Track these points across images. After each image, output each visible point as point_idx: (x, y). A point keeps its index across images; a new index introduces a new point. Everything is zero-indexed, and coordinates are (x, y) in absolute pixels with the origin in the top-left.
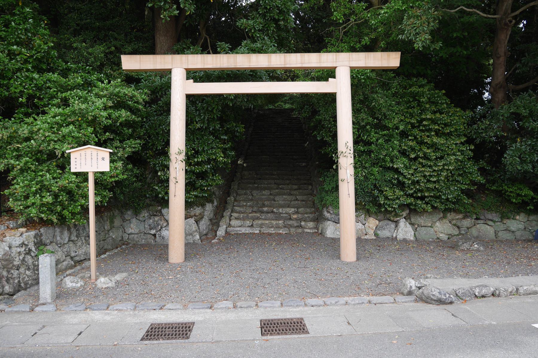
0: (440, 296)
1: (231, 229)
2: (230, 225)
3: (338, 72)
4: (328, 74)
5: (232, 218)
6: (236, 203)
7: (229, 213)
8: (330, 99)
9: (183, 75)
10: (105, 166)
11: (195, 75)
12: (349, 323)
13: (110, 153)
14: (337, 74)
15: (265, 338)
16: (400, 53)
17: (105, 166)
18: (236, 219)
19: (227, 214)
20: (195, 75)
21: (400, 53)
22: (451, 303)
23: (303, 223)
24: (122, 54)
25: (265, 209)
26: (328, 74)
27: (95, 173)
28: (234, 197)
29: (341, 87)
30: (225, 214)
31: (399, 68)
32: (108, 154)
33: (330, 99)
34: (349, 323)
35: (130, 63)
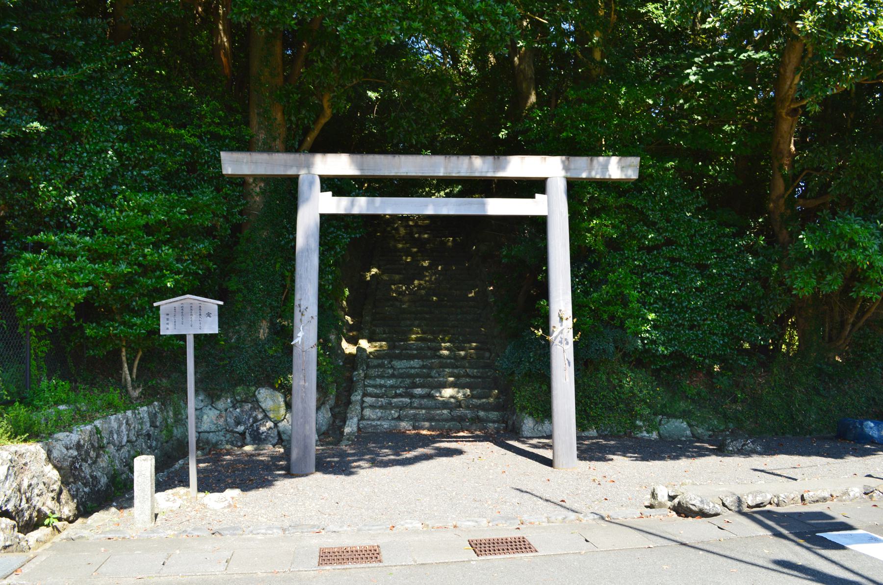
0: (701, 506)
1: (365, 422)
2: (362, 418)
3: (550, 185)
4: (532, 187)
5: (365, 405)
6: (367, 382)
7: (359, 397)
8: (539, 224)
9: (322, 188)
10: (211, 327)
11: (335, 185)
12: (587, 541)
13: (219, 305)
14: (545, 186)
15: (481, 558)
16: (639, 159)
17: (211, 327)
18: (372, 407)
19: (356, 397)
20: (335, 185)
21: (639, 159)
22: (716, 515)
23: (482, 414)
24: (223, 150)
25: (418, 391)
26: (532, 187)
27: (197, 337)
28: (363, 370)
29: (553, 207)
30: (353, 398)
31: (636, 180)
32: (216, 307)
33: (539, 224)
34: (587, 541)
35: (233, 164)
